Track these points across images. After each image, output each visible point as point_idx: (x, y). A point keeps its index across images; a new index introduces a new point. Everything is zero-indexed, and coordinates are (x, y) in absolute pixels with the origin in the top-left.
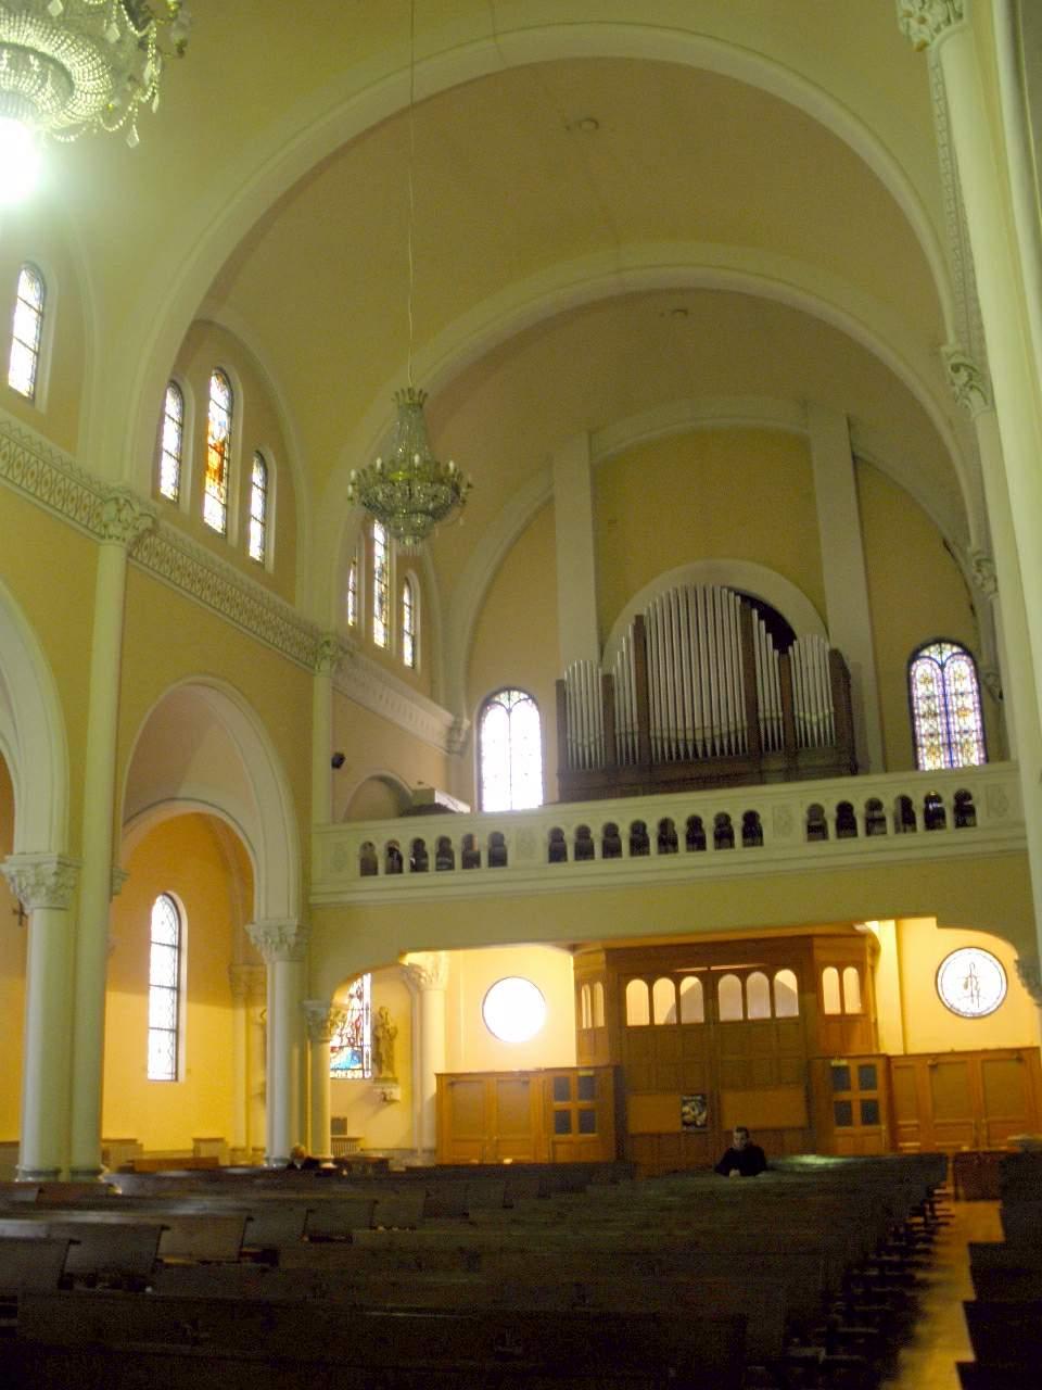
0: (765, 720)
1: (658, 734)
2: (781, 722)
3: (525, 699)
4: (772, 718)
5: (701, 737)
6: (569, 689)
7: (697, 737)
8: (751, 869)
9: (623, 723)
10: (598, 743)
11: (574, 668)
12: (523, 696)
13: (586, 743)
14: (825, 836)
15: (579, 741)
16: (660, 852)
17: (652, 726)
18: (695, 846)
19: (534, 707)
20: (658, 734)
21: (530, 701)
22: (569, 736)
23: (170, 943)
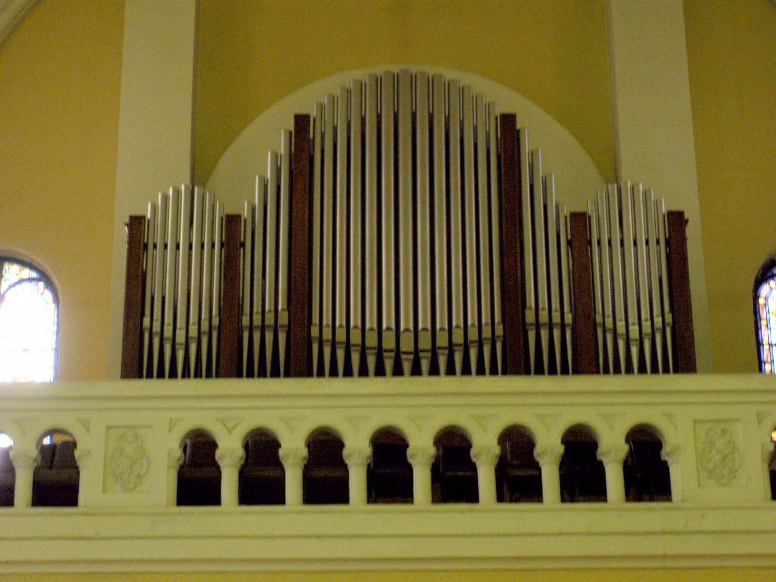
0: (538, 326)
1: (327, 334)
2: (499, 346)
3: (31, 280)
4: (398, 352)
5: (411, 348)
6: (314, 132)
7: (385, 345)
8: (655, 546)
9: (257, 307)
10: (193, 347)
11: (165, 198)
12: (27, 273)
13: (181, 338)
14: (215, 500)
15: (168, 332)
16: (500, 498)
17: (316, 319)
18: (587, 497)
19: (48, 295)
20: (327, 334)
21: (41, 284)
22: (147, 321)
23: (603, 311)
